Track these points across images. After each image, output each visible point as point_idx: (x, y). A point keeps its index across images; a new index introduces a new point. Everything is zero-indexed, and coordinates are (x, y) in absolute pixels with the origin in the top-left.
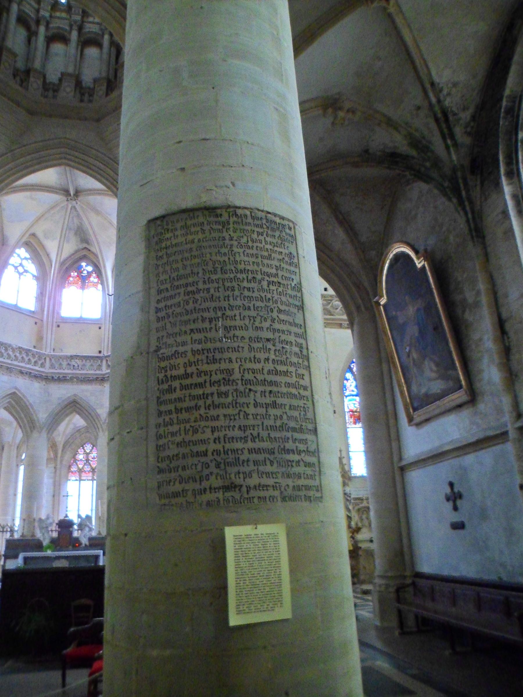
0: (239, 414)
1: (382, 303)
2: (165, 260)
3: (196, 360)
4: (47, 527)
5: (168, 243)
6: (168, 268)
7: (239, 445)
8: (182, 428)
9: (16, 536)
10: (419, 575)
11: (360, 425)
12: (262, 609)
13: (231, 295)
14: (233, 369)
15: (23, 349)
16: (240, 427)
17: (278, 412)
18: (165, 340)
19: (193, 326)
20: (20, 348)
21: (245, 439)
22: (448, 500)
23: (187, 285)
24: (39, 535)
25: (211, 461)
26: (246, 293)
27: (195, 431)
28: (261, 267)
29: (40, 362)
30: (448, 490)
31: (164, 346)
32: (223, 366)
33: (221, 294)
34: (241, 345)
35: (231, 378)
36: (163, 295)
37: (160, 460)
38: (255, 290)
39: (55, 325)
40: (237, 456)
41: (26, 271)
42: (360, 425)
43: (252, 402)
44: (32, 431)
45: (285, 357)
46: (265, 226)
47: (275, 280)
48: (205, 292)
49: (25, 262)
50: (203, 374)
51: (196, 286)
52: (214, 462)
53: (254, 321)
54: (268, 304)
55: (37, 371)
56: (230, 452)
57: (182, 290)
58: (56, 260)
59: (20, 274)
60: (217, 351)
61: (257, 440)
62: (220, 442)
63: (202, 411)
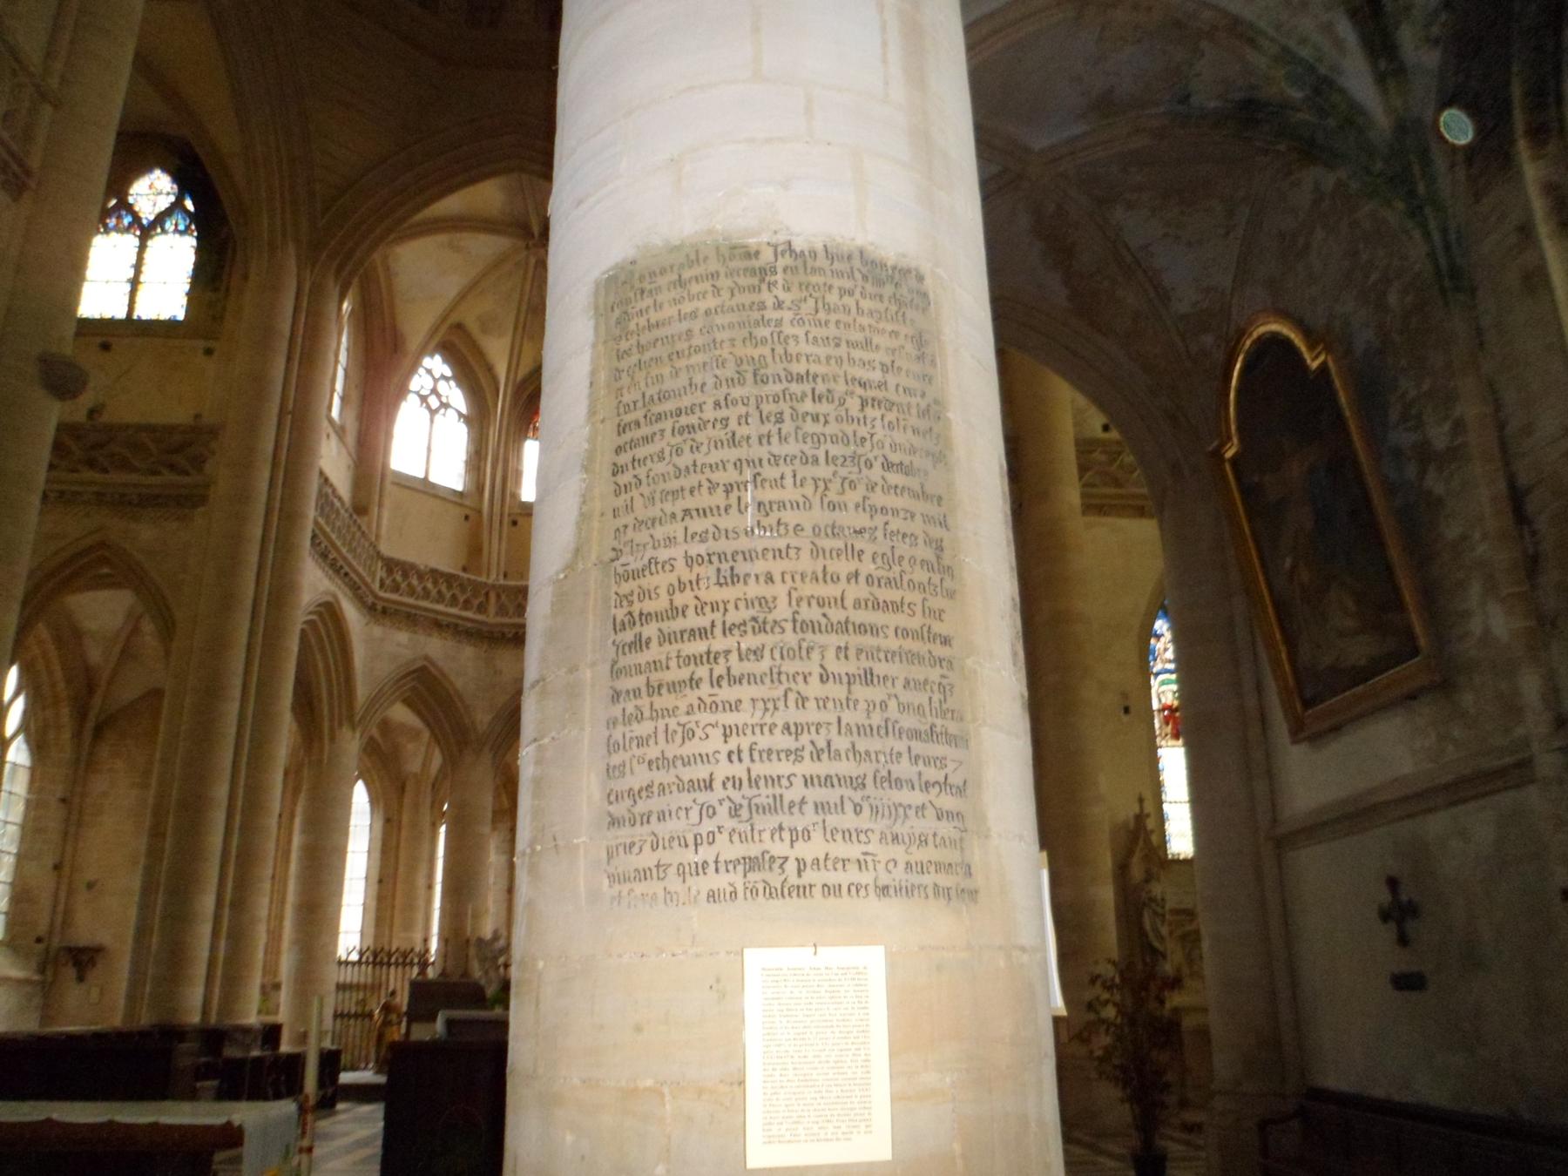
0: (786, 695)
1: (1229, 454)
2: (634, 359)
3: (694, 578)
4: (496, 958)
5: (642, 321)
6: (640, 376)
7: (783, 768)
8: (661, 729)
9: (431, 973)
10: (1319, 1095)
11: (1180, 742)
12: (822, 1136)
13: (774, 431)
14: (775, 599)
15: (442, 574)
16: (787, 728)
17: (876, 693)
18: (630, 533)
19: (690, 503)
20: (434, 571)
21: (796, 755)
22: (1385, 916)
23: (679, 413)
24: (477, 972)
25: (721, 802)
26: (810, 427)
27: (689, 735)
28: (845, 366)
29: (476, 602)
30: (1385, 897)
31: (627, 549)
32: (754, 590)
33: (753, 429)
34: (794, 542)
35: (770, 618)
36: (628, 436)
37: (613, 798)
38: (831, 419)
39: (506, 520)
40: (778, 791)
41: (445, 406)
42: (1180, 742)
43: (817, 670)
44: (461, 751)
45: (897, 569)
46: (858, 275)
47: (879, 394)
48: (718, 426)
49: (442, 387)
50: (708, 609)
51: (698, 414)
52: (727, 804)
53: (826, 488)
54: (860, 451)
55: (472, 621)
56: (762, 783)
57: (667, 425)
58: (507, 378)
59: (433, 412)
60: (740, 557)
61: (825, 756)
62: (740, 760)
63: (705, 690)
